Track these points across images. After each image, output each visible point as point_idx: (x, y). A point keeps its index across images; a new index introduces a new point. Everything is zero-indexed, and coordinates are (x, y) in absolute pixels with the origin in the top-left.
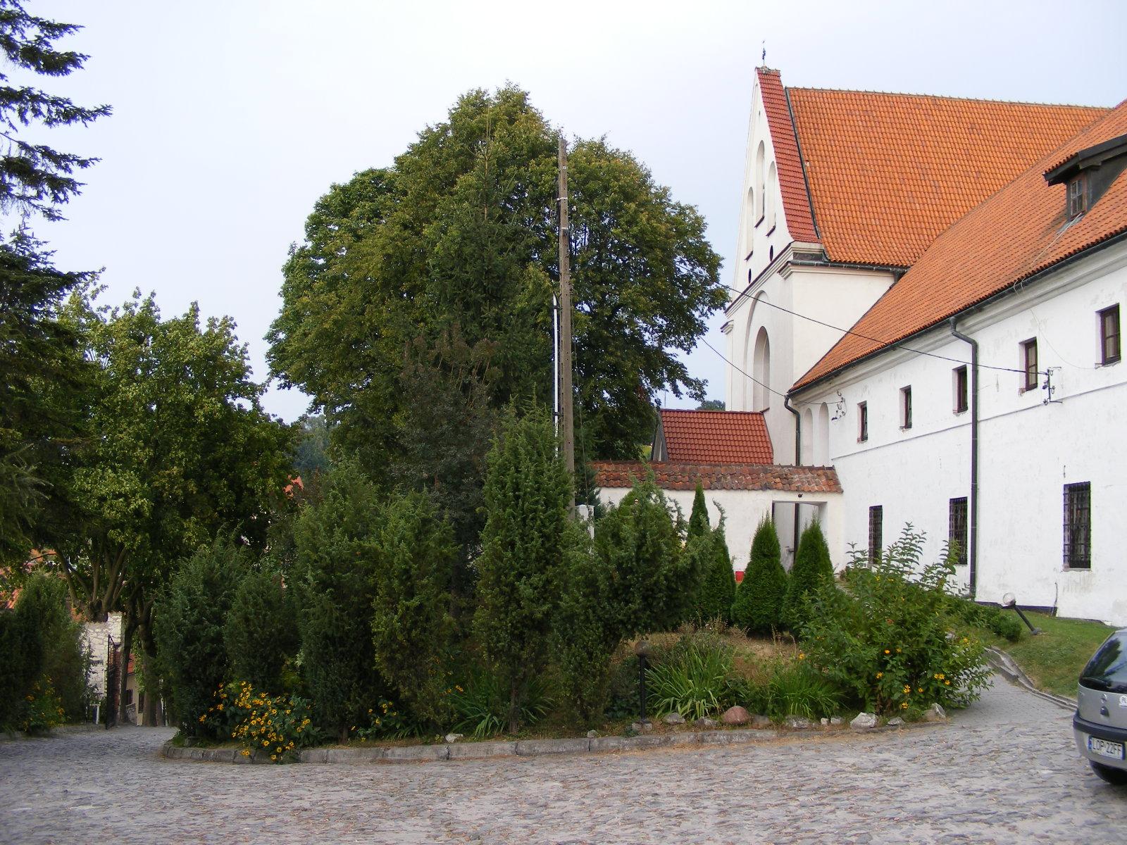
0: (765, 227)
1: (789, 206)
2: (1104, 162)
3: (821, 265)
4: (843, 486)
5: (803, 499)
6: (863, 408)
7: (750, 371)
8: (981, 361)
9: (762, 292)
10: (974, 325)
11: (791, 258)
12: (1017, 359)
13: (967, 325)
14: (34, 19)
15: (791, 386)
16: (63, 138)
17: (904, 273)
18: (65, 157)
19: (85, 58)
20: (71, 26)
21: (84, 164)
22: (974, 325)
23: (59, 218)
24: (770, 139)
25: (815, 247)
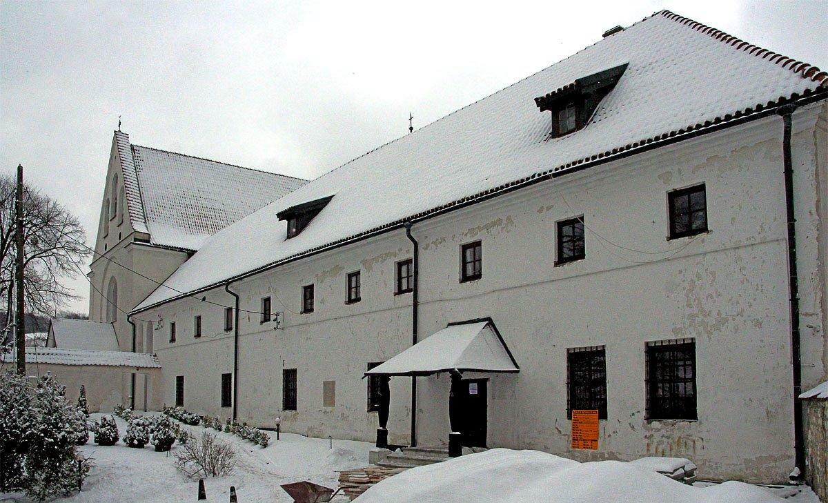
6: (173, 325)
12: (259, 307)
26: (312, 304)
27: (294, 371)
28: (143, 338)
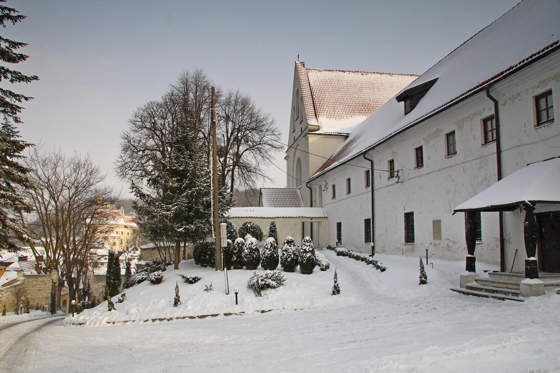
2: (418, 93)
6: (334, 186)
7: (295, 176)
8: (375, 167)
12: (387, 167)
14: (6, 39)
16: (18, 88)
18: (18, 96)
19: (27, 57)
20: (22, 43)
21: (26, 99)
23: (20, 122)
26: (454, 148)
27: (412, 214)
28: (316, 197)
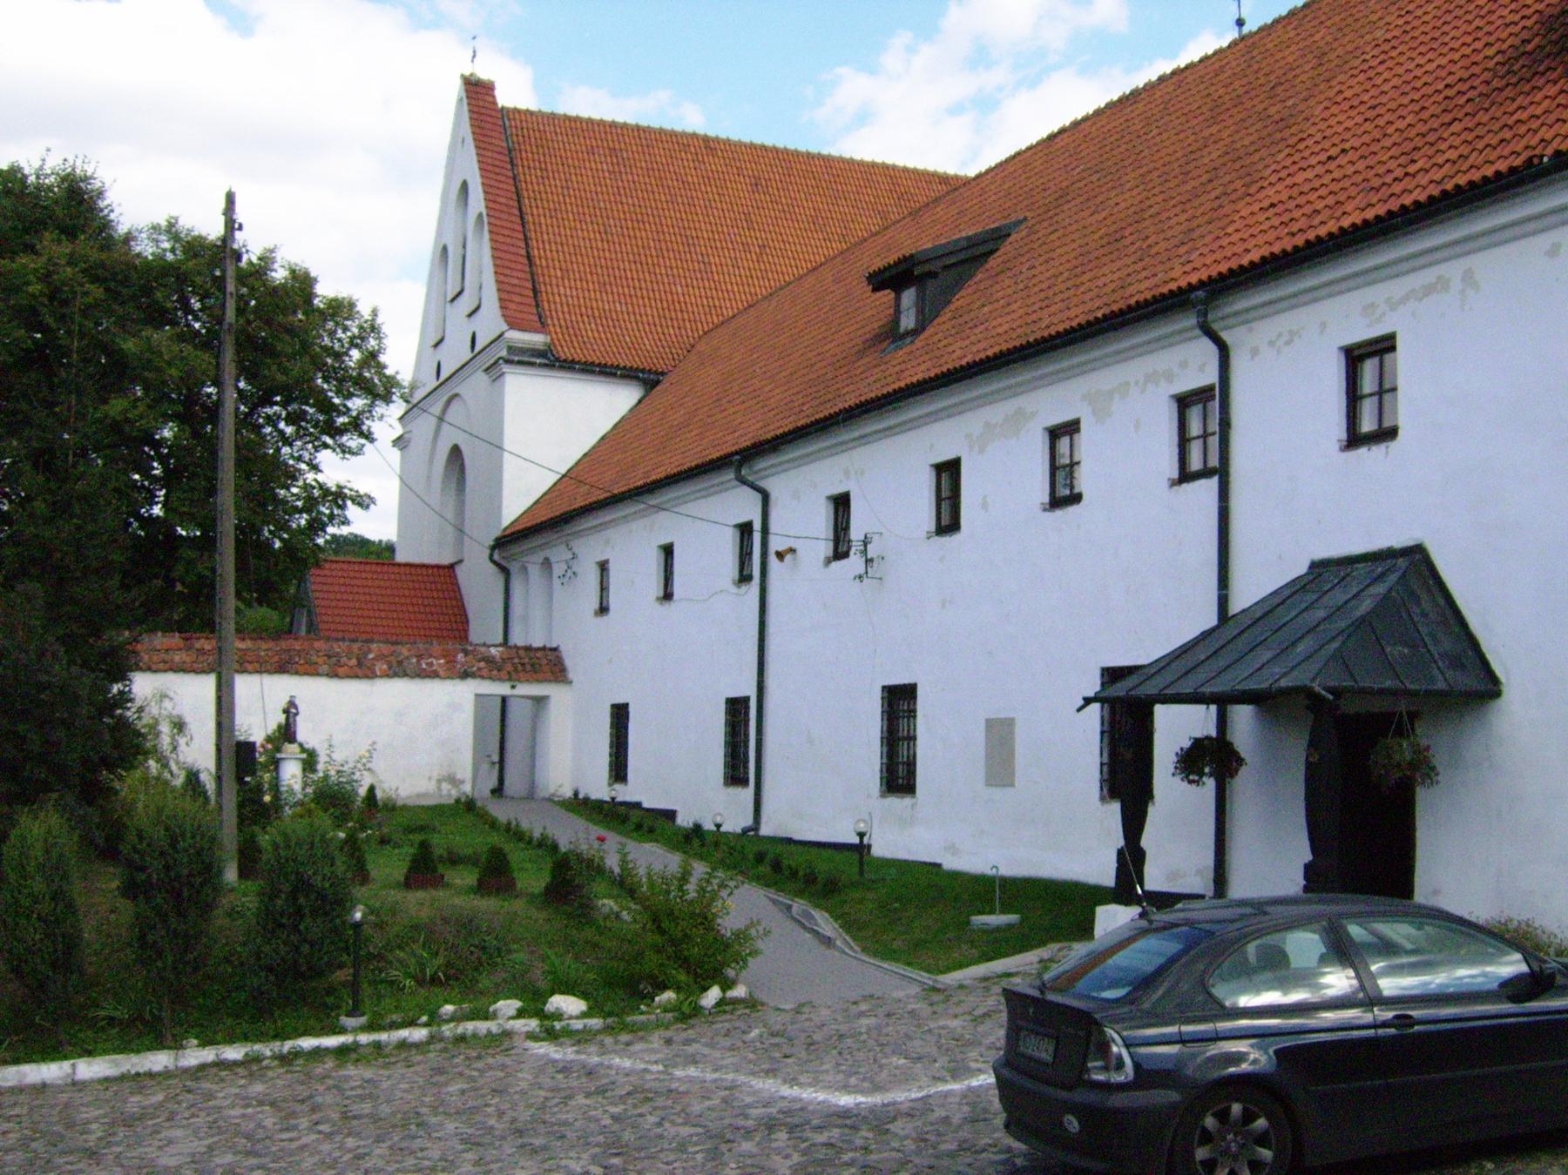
0: (466, 303)
1: (502, 278)
3: (546, 365)
4: (571, 675)
5: (517, 692)
6: (603, 567)
9: (456, 395)
10: (765, 469)
11: (504, 353)
12: (821, 521)
13: (756, 468)
15: (497, 533)
17: (658, 382)
22: (765, 469)
24: (479, 180)
25: (537, 339)
